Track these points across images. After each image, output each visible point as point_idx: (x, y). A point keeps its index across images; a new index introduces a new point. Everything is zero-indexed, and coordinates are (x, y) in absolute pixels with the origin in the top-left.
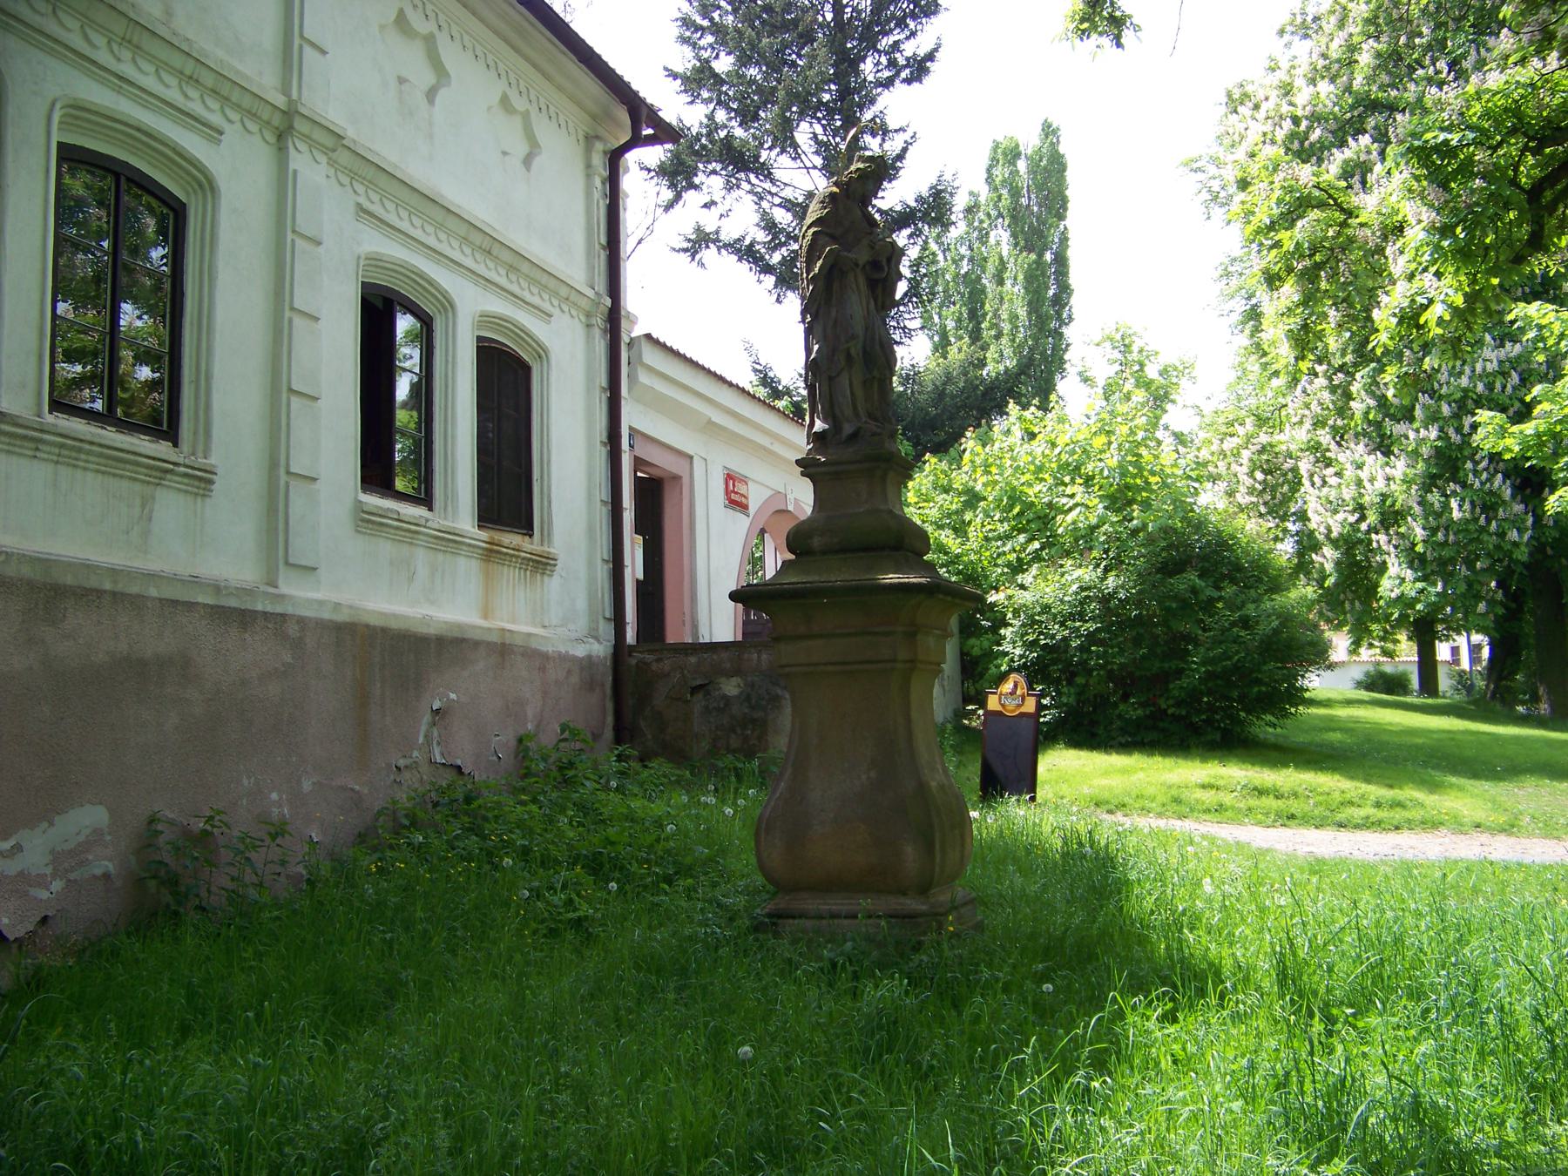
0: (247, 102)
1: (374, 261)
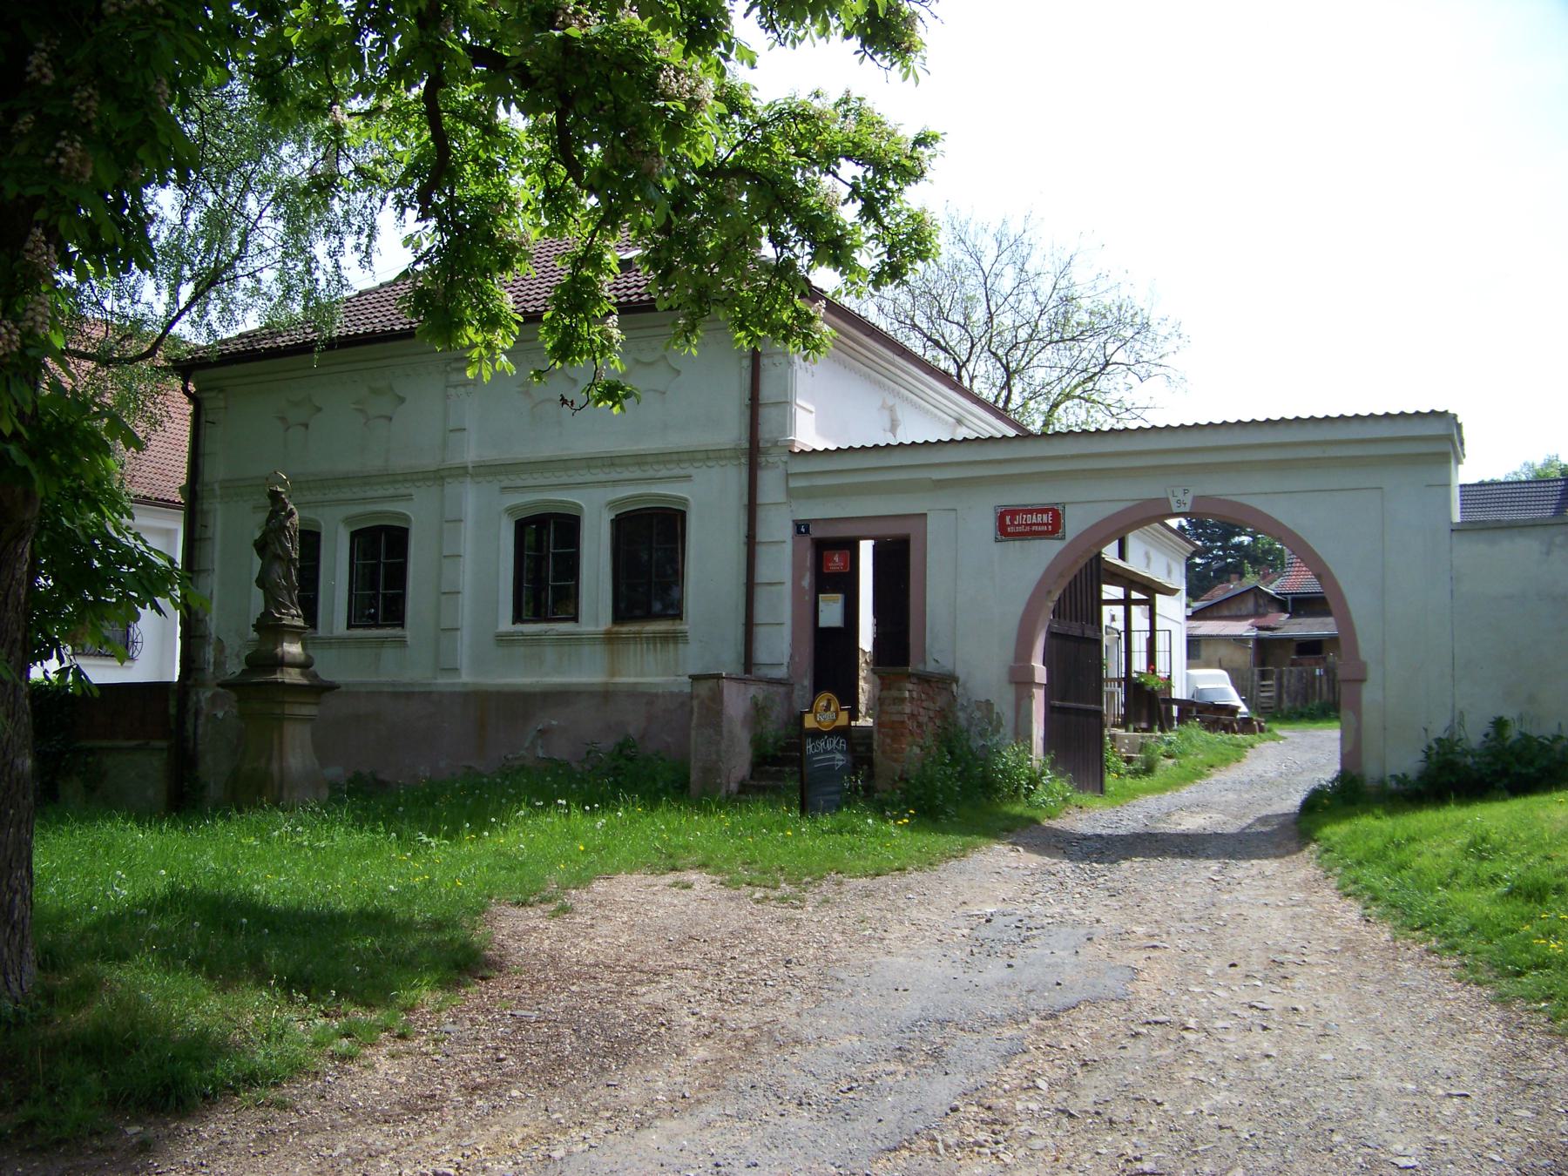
0: (675, 457)
1: (612, 504)
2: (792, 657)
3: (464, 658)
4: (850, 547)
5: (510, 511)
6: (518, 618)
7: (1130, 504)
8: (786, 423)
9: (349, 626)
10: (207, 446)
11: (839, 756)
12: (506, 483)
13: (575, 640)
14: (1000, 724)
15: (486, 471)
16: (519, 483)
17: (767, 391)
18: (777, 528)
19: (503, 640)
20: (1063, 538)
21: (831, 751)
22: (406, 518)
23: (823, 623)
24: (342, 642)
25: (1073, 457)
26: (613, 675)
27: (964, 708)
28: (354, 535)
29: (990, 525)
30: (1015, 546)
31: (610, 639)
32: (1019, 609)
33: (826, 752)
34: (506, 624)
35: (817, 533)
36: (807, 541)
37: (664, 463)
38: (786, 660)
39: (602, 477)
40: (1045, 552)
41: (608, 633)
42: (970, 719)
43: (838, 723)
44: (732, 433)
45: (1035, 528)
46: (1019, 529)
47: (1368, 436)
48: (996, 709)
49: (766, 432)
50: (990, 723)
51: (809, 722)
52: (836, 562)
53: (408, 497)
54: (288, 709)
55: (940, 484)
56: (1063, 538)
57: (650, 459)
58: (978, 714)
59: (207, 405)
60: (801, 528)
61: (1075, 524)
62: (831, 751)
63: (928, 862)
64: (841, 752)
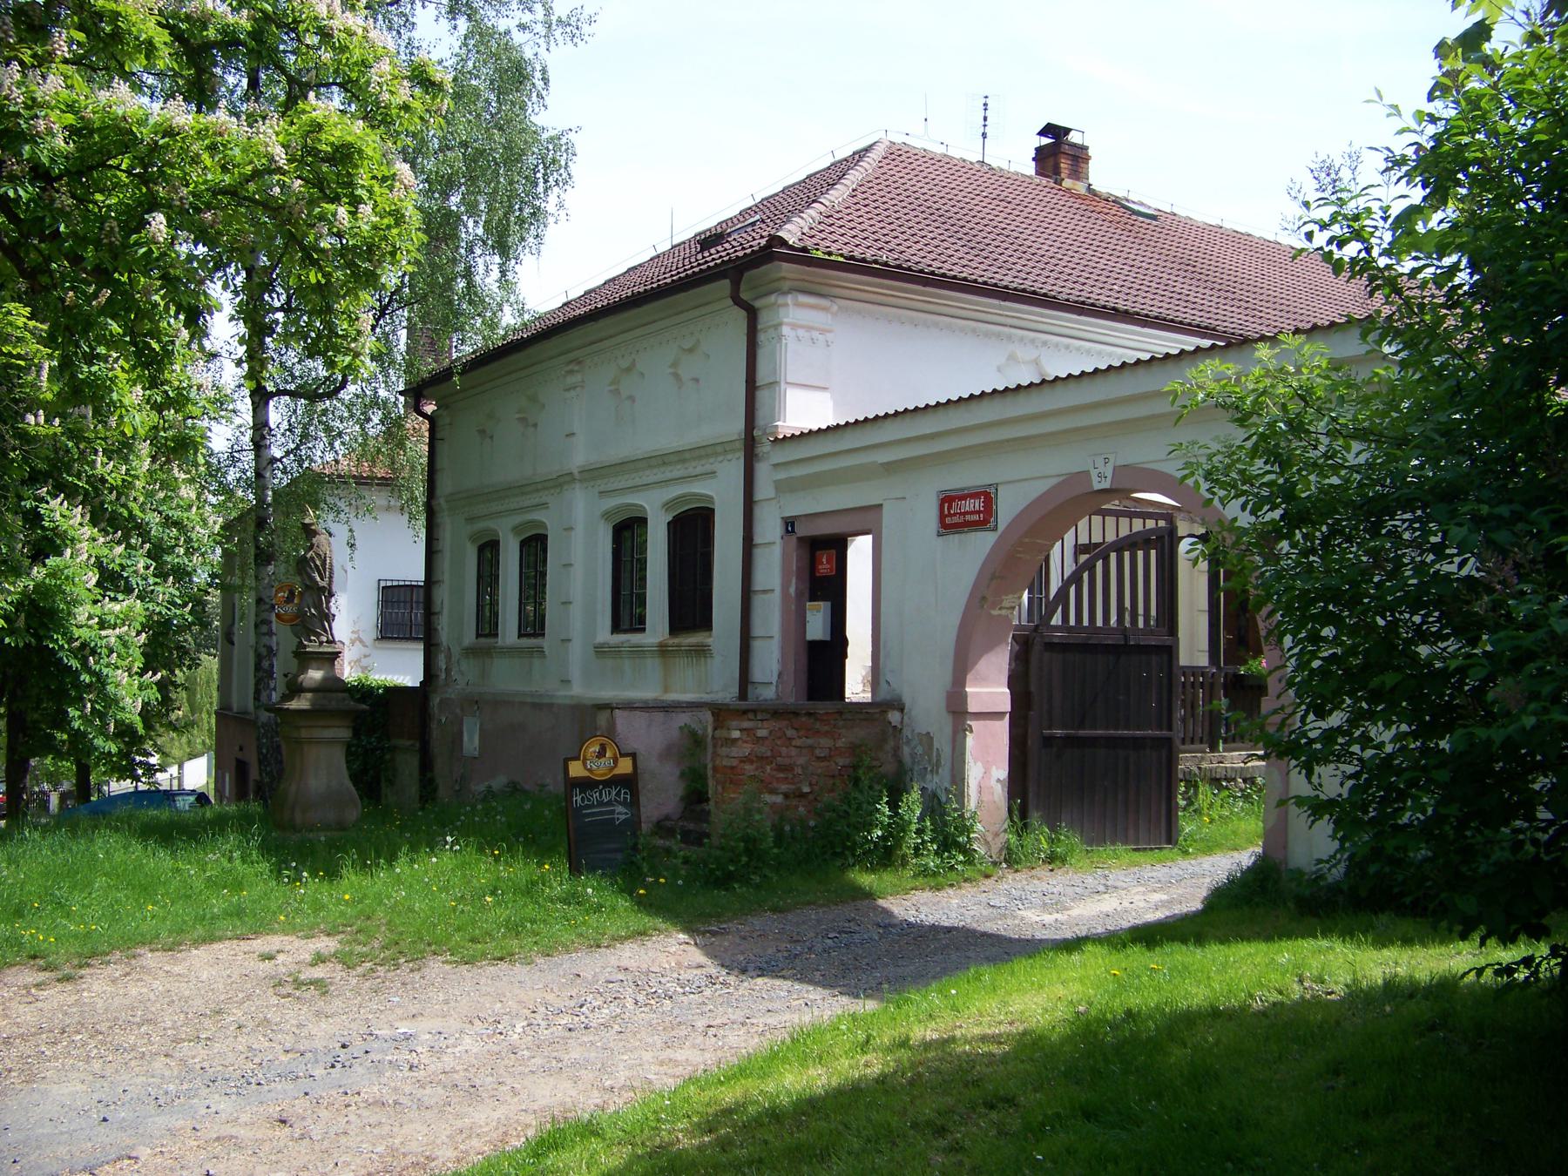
2: (780, 675)
3: (575, 673)
4: (839, 546)
5: (606, 515)
6: (616, 627)
7: (1054, 481)
8: (776, 411)
9: (520, 636)
10: (442, 462)
11: (620, 809)
12: (602, 488)
13: (638, 652)
14: (938, 764)
15: (592, 474)
16: (638, 481)
17: (762, 376)
18: (769, 529)
19: (601, 651)
20: (995, 529)
21: (609, 803)
22: (543, 525)
23: (809, 637)
24: (511, 651)
25: (908, 440)
26: (666, 690)
27: (908, 742)
28: (523, 544)
29: (927, 513)
30: (954, 539)
31: (663, 651)
32: (954, 619)
33: (601, 804)
34: (604, 634)
35: (802, 530)
36: (794, 538)
37: (700, 458)
38: (774, 679)
39: (660, 477)
40: (980, 544)
41: (661, 645)
42: (913, 755)
43: (617, 771)
44: (735, 426)
45: (968, 517)
46: (956, 520)
47: (1112, 396)
48: (936, 745)
49: (760, 420)
50: (930, 761)
51: (576, 770)
52: (825, 567)
53: (544, 505)
54: (304, 733)
55: (890, 468)
56: (995, 529)
57: (687, 455)
58: (919, 750)
59: (440, 422)
60: (790, 525)
61: (1008, 508)
62: (609, 803)
63: (473, 945)
64: (624, 804)
